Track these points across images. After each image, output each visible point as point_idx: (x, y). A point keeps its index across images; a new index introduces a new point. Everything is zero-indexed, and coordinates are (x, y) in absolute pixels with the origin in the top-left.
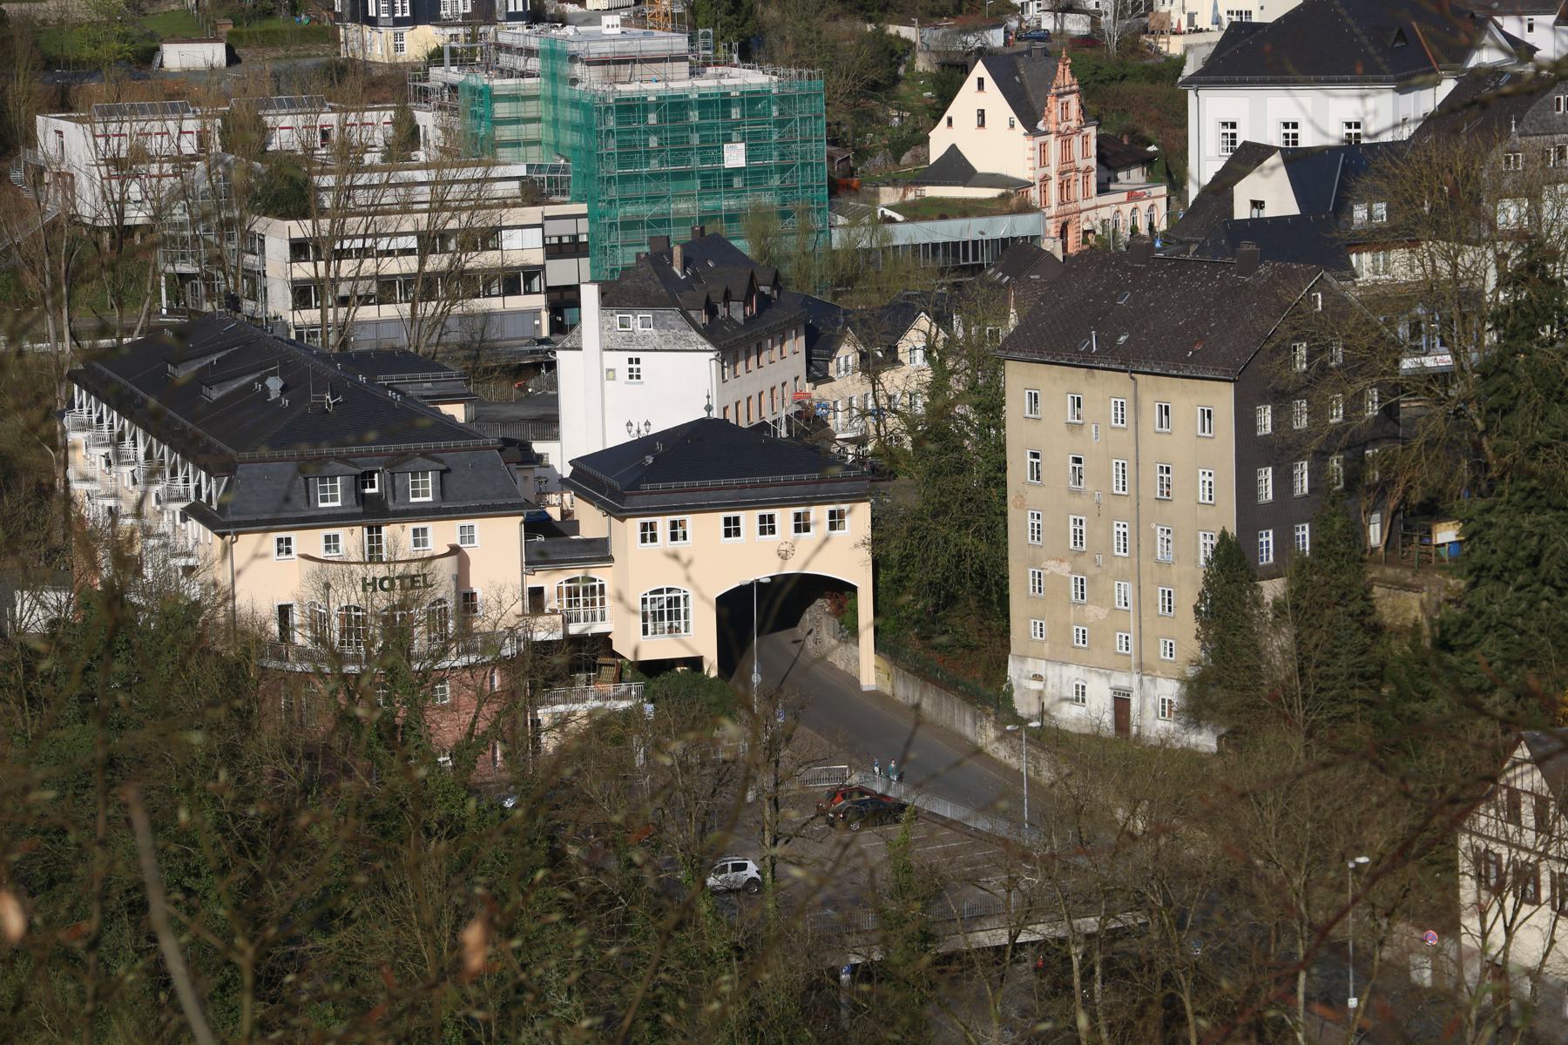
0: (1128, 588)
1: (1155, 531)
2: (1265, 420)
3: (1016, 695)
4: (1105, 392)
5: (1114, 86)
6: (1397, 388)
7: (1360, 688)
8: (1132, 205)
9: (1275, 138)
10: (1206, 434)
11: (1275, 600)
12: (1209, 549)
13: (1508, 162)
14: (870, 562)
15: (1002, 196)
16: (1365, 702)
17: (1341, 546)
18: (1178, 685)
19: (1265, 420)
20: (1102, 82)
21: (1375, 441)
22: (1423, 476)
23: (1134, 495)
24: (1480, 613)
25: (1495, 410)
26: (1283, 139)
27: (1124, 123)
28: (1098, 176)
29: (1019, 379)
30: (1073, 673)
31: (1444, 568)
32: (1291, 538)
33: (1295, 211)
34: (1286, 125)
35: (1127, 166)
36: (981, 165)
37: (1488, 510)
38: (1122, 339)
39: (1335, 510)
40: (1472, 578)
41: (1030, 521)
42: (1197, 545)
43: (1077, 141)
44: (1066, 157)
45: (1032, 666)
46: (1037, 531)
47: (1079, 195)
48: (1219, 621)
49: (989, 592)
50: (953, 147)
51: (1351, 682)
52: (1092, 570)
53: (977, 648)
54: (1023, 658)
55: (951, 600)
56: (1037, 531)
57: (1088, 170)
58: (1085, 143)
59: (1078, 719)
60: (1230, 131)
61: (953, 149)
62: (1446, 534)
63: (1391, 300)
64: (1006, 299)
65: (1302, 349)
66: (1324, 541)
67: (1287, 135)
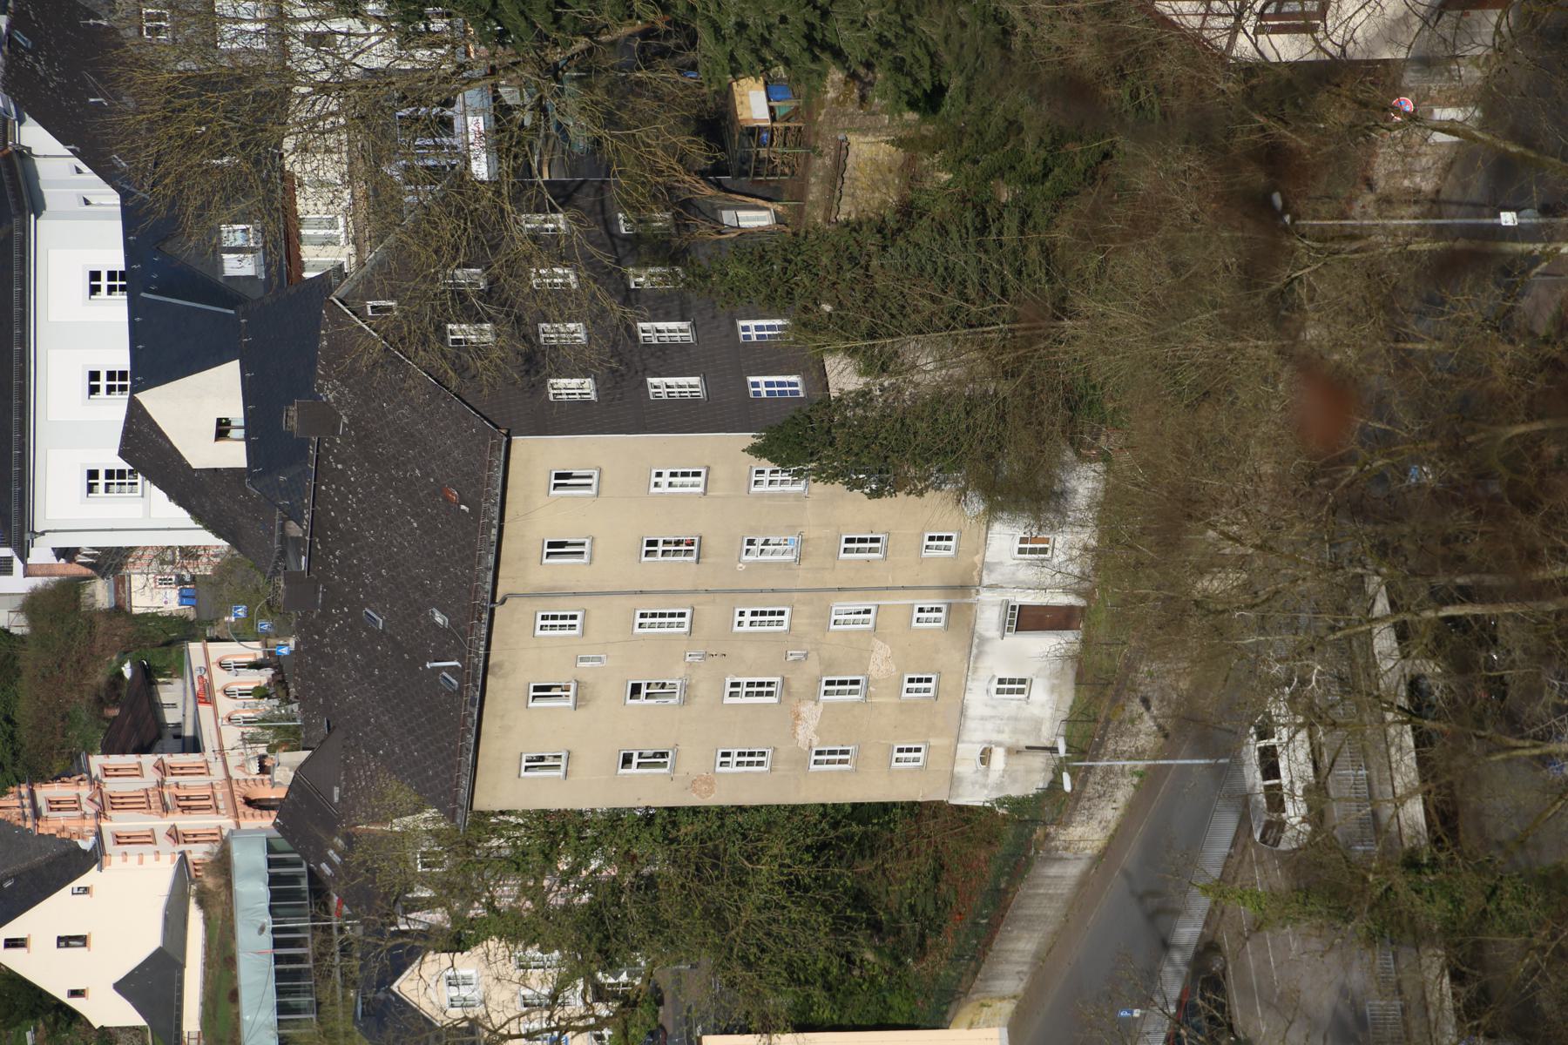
0: (841, 606)
1: (748, 564)
2: (571, 387)
3: (1016, 791)
4: (523, 647)
5: (23, 734)
6: (518, 184)
7: (1000, 233)
8: (220, 698)
9: (114, 409)
10: (593, 481)
11: (861, 373)
12: (778, 477)
13: (158, 30)
14: (800, 1036)
15: (201, 903)
16: (1023, 223)
17: (775, 272)
18: (997, 527)
19: (571, 387)
20: (15, 754)
21: (608, 224)
22: (663, 140)
23: (691, 599)
24: (882, 41)
25: (557, 18)
26: (116, 394)
27: (85, 717)
28: (171, 752)
29: (506, 786)
30: (979, 698)
31: (808, 105)
32: (762, 346)
33: (233, 368)
34: (94, 390)
35: (156, 708)
36: (150, 940)
37: (717, 29)
38: (439, 618)
39: (710, 279)
40: (826, 57)
41: (735, 769)
42: (772, 496)
43: (112, 786)
44: (140, 803)
45: (967, 766)
46: (750, 757)
47: (203, 780)
48: (893, 458)
49: (849, 838)
50: (120, 987)
51: (991, 246)
52: (813, 667)
53: (937, 859)
54: (954, 781)
55: (859, 898)
56: (750, 757)
57: (161, 768)
58: (117, 772)
59: (1053, 689)
60: (102, 480)
61: (122, 987)
62: (753, 103)
63: (377, 209)
64: (377, 840)
65: (458, 330)
66: (765, 291)
67: (110, 389)
